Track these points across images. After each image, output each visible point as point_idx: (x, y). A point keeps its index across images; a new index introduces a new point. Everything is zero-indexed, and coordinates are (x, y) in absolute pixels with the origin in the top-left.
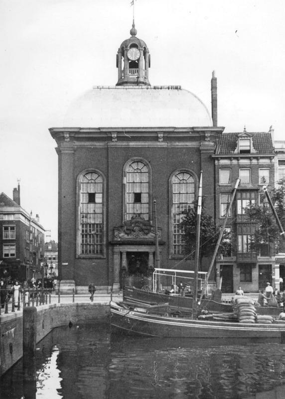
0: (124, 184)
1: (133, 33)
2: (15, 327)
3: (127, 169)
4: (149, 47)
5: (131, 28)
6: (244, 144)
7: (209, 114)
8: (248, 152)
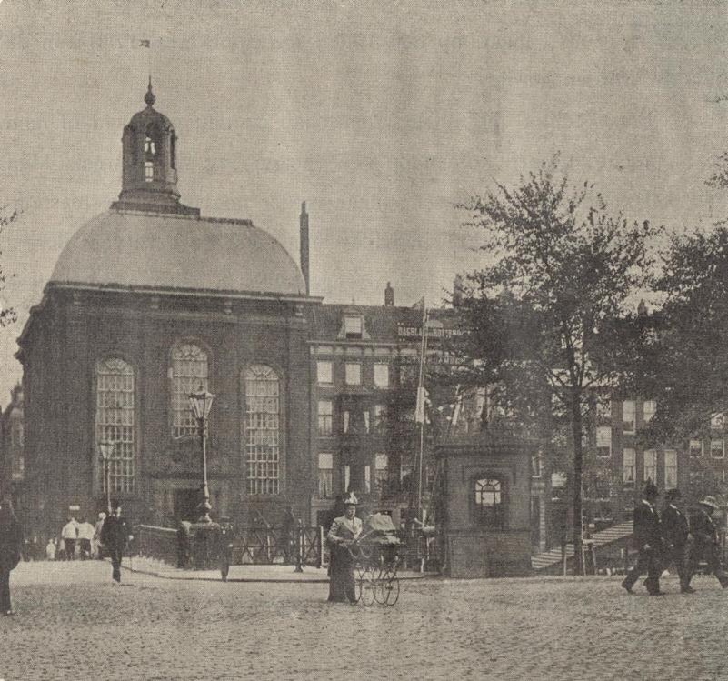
0: (170, 380)
1: (150, 99)
2: (344, 538)
3: (177, 356)
4: (177, 133)
5: (147, 90)
6: (353, 325)
7: (297, 268)
8: (358, 336)
